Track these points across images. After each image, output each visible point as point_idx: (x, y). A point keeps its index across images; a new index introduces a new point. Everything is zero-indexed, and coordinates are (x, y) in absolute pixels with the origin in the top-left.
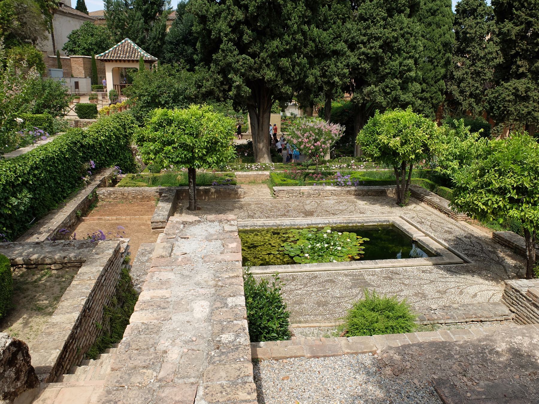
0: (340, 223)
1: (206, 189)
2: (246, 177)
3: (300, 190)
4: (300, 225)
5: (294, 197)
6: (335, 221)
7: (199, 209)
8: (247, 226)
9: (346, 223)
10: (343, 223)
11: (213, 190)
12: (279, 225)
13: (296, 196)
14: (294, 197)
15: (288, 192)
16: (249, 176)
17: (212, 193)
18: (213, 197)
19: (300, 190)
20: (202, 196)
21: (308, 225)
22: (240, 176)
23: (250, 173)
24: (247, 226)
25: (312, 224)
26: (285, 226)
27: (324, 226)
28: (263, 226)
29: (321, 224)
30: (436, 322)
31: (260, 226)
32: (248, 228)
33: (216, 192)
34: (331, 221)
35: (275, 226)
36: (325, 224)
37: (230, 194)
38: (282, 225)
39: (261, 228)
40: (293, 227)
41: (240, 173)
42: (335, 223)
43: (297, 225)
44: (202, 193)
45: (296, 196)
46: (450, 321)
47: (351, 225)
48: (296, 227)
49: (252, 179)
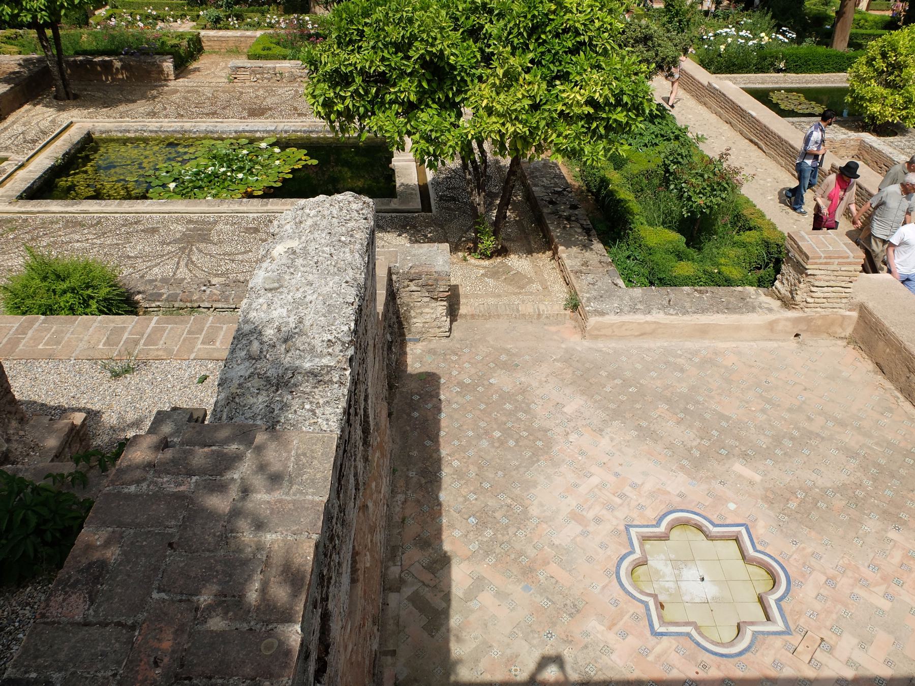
0: (294, 131)
1: (106, 61)
2: (220, 40)
3: (275, 68)
4: (223, 132)
5: (266, 81)
6: (286, 128)
7: (76, 97)
8: (129, 131)
9: (305, 132)
10: (300, 131)
11: (118, 64)
12: (185, 131)
13: (269, 80)
14: (266, 81)
15: (253, 72)
16: (226, 40)
17: (117, 69)
18: (120, 76)
19: (275, 68)
20: (100, 74)
21: (236, 132)
22: (210, 39)
23: (229, 33)
24: (129, 131)
25: (244, 131)
26: (195, 133)
27: (265, 135)
28: (156, 132)
29: (260, 131)
30: (196, 305)
31: (151, 131)
32: (132, 135)
33: (123, 67)
34: (281, 127)
35: (179, 132)
36: (268, 132)
37: (149, 72)
38: (190, 131)
39: (153, 135)
40: (210, 135)
41: (212, 33)
42: (286, 132)
43: (217, 132)
44: (99, 68)
45: (269, 80)
46: (220, 305)
47: (314, 135)
48: (216, 136)
49: (231, 44)
